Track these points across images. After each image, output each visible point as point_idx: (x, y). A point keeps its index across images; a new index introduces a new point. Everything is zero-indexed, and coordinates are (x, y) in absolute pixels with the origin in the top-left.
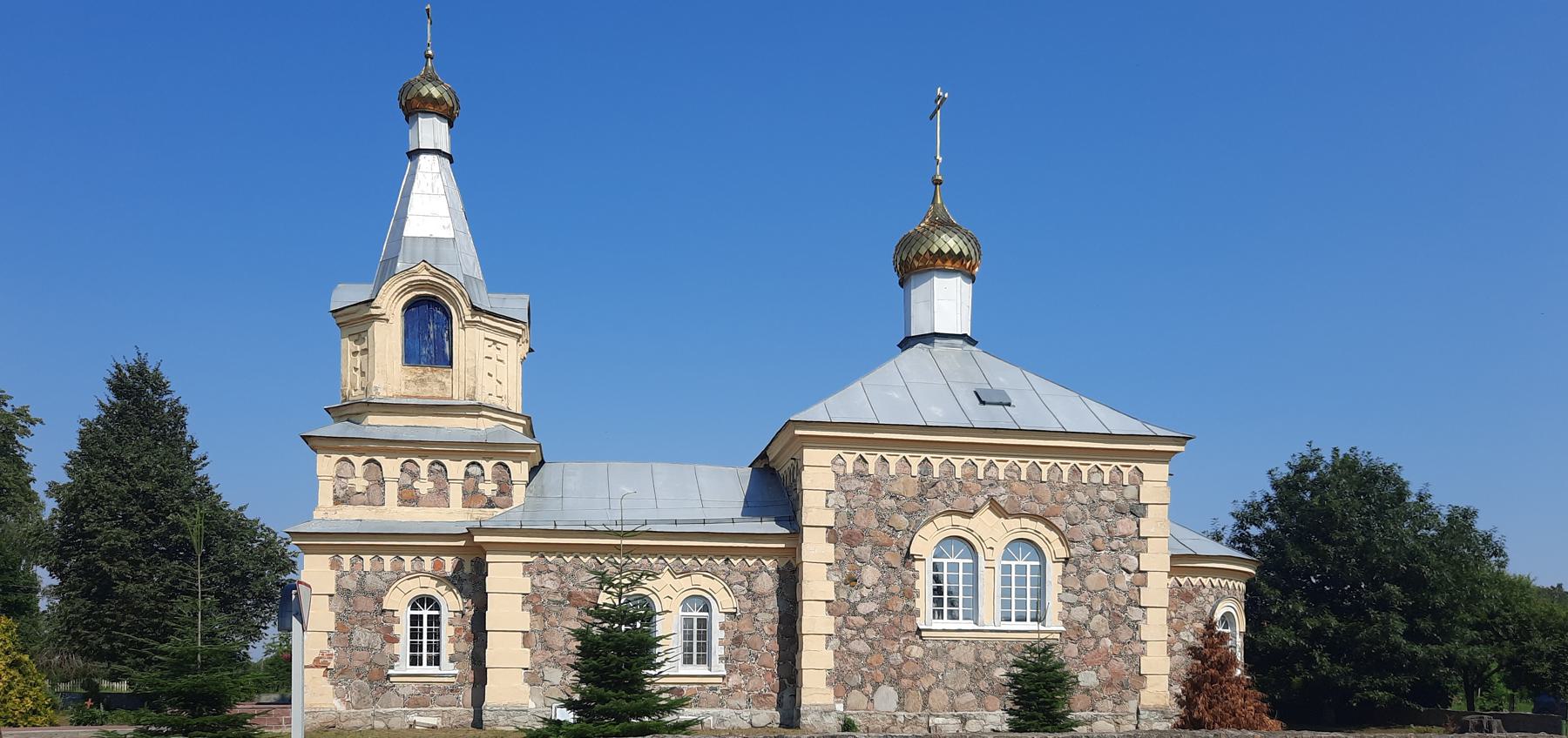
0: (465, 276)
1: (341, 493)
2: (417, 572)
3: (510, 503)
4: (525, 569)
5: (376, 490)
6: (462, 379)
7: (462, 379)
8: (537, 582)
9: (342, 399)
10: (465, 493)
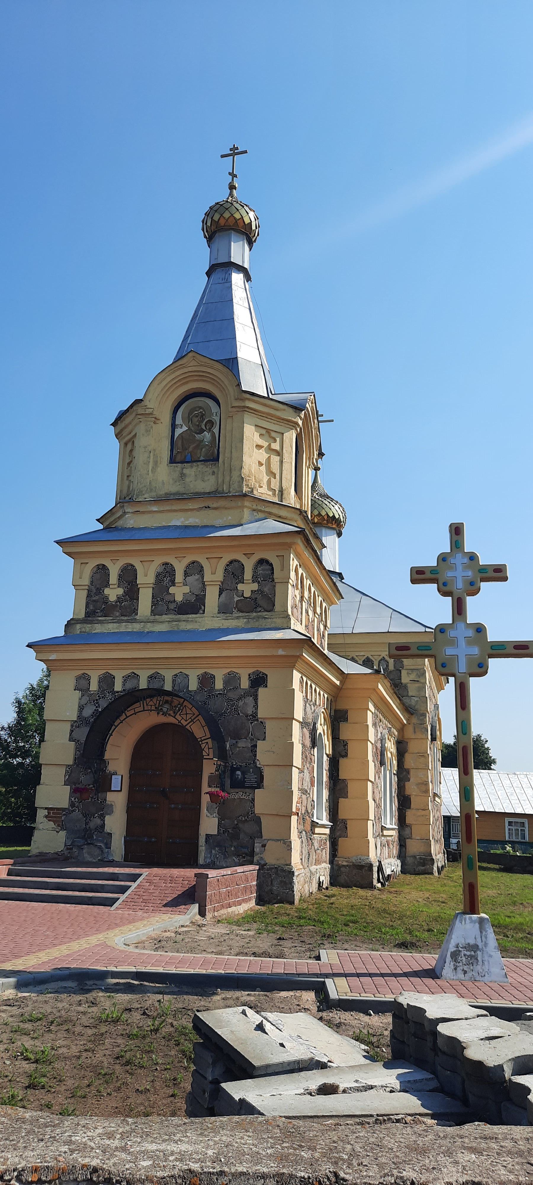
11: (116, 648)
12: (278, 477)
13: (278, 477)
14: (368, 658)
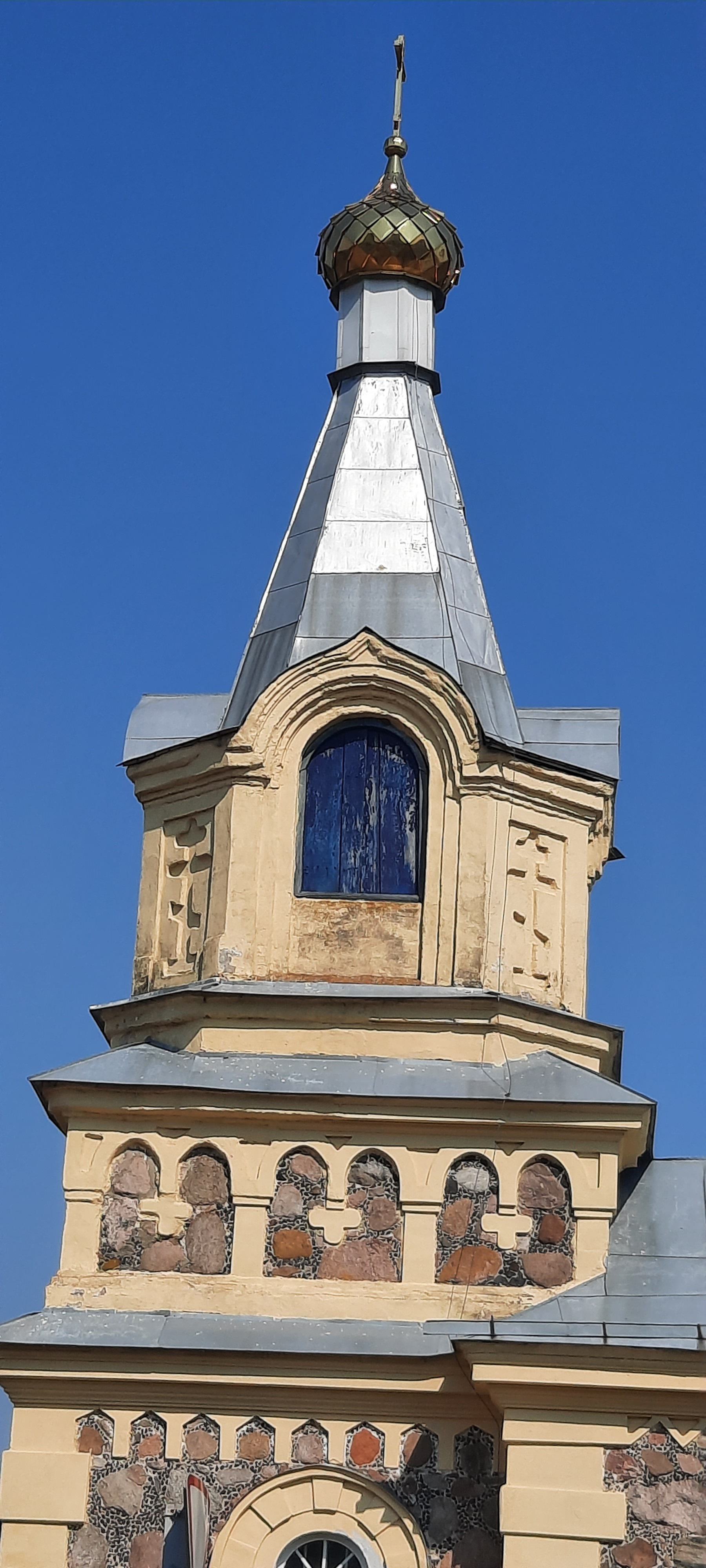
0: (462, 665)
2: (309, 1466)
3: (565, 1274)
4: (612, 1466)
6: (447, 931)
7: (447, 931)
8: (644, 1507)
9: (136, 985)
10: (444, 1242)
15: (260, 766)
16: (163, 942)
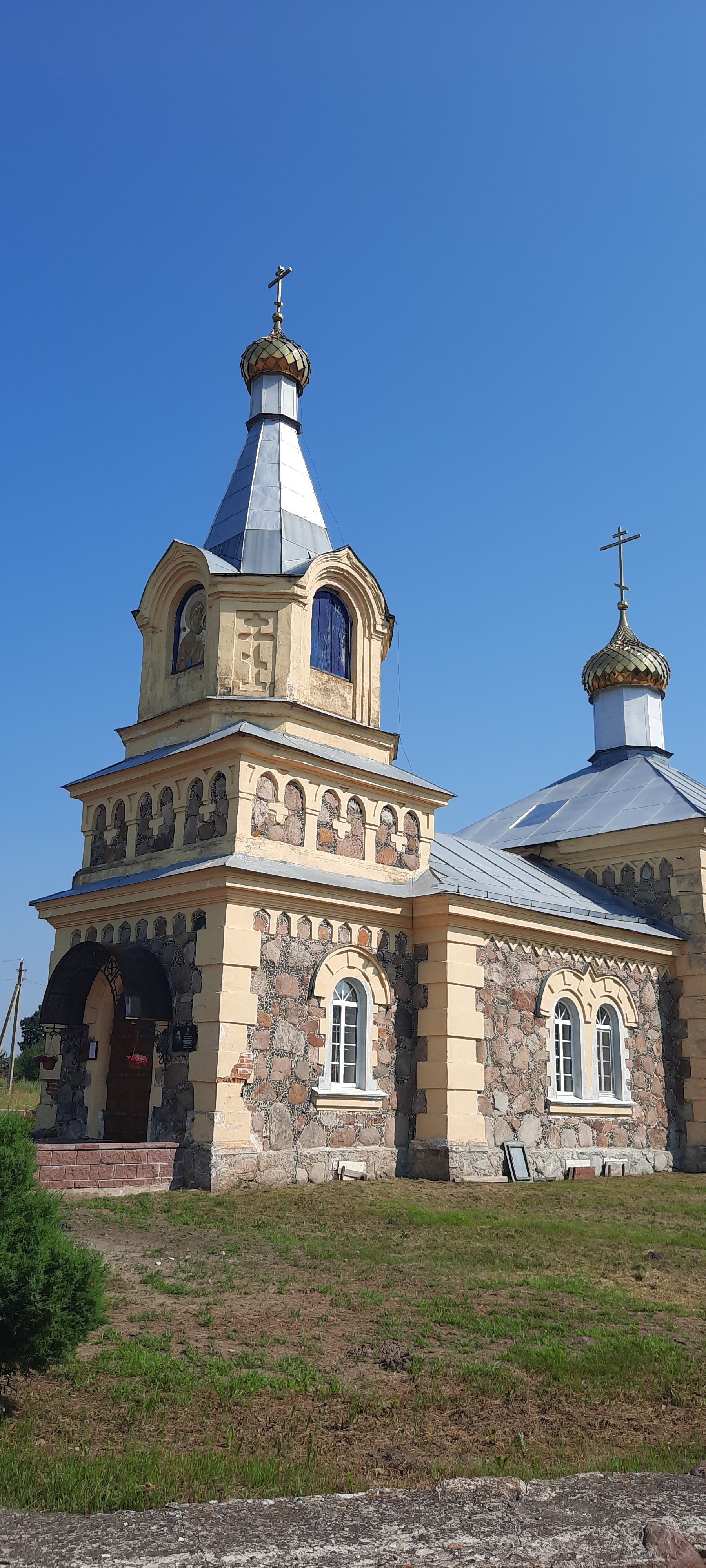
1: (260, 821)
4: (478, 954)
5: (295, 822)
11: (101, 896)
12: (270, 666)
13: (270, 666)
14: (627, 866)
15: (305, 598)
16: (239, 671)
